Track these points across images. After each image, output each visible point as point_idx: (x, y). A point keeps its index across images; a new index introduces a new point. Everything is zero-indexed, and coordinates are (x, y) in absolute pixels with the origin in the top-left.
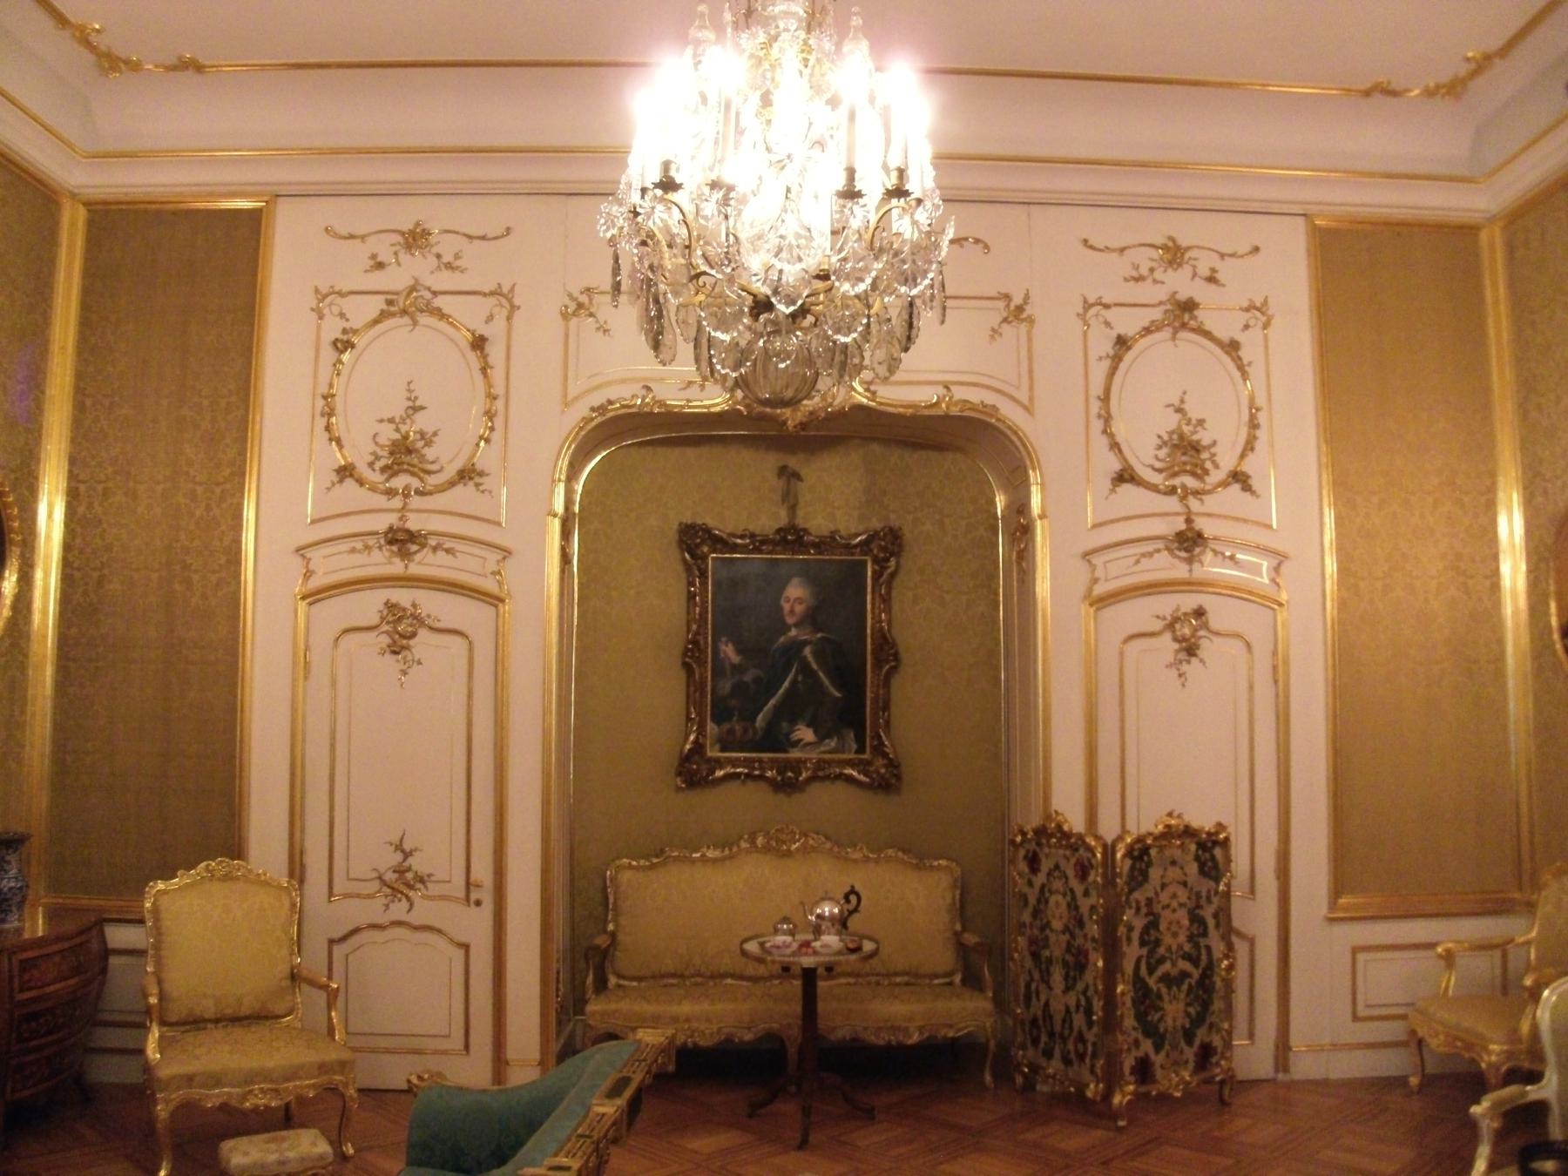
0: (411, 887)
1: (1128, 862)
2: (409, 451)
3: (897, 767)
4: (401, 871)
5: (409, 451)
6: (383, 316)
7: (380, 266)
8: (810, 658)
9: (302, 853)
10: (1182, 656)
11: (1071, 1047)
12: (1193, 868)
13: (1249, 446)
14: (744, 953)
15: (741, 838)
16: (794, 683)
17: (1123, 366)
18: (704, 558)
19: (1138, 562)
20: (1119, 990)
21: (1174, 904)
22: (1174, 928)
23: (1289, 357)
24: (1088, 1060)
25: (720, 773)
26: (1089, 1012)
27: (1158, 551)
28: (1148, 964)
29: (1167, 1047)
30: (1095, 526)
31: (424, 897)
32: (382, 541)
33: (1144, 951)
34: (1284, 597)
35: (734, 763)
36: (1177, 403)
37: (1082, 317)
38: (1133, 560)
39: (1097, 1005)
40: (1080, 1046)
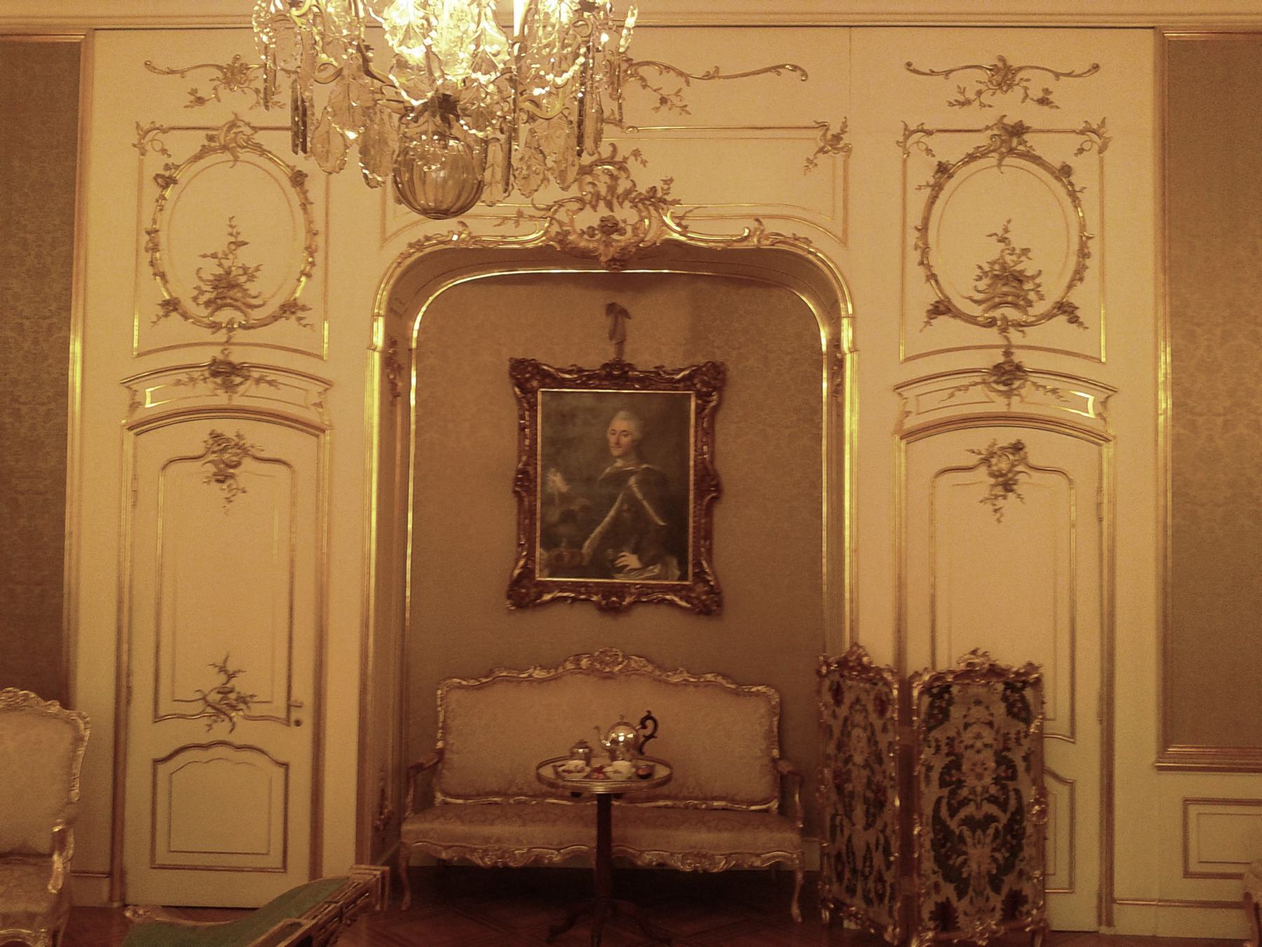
0: (234, 708)
1: (926, 700)
2: (232, 286)
3: (718, 594)
4: (224, 692)
5: (232, 286)
6: (204, 152)
7: (200, 101)
8: (635, 489)
9: (129, 675)
10: (999, 491)
11: (871, 885)
12: (1000, 709)
13: (1078, 276)
14: (539, 778)
15: (566, 661)
16: (619, 511)
17: (943, 195)
18: (534, 392)
19: (952, 395)
20: (916, 832)
21: (979, 744)
22: (979, 770)
23: (1127, 191)
24: (886, 902)
25: (547, 597)
26: (887, 852)
27: (976, 384)
28: (949, 804)
29: (971, 893)
30: (907, 359)
31: (247, 718)
32: (207, 374)
33: (946, 791)
34: (1111, 431)
35: (561, 587)
36: (1000, 232)
37: (902, 144)
38: (946, 394)
39: (895, 844)
40: (880, 886)
